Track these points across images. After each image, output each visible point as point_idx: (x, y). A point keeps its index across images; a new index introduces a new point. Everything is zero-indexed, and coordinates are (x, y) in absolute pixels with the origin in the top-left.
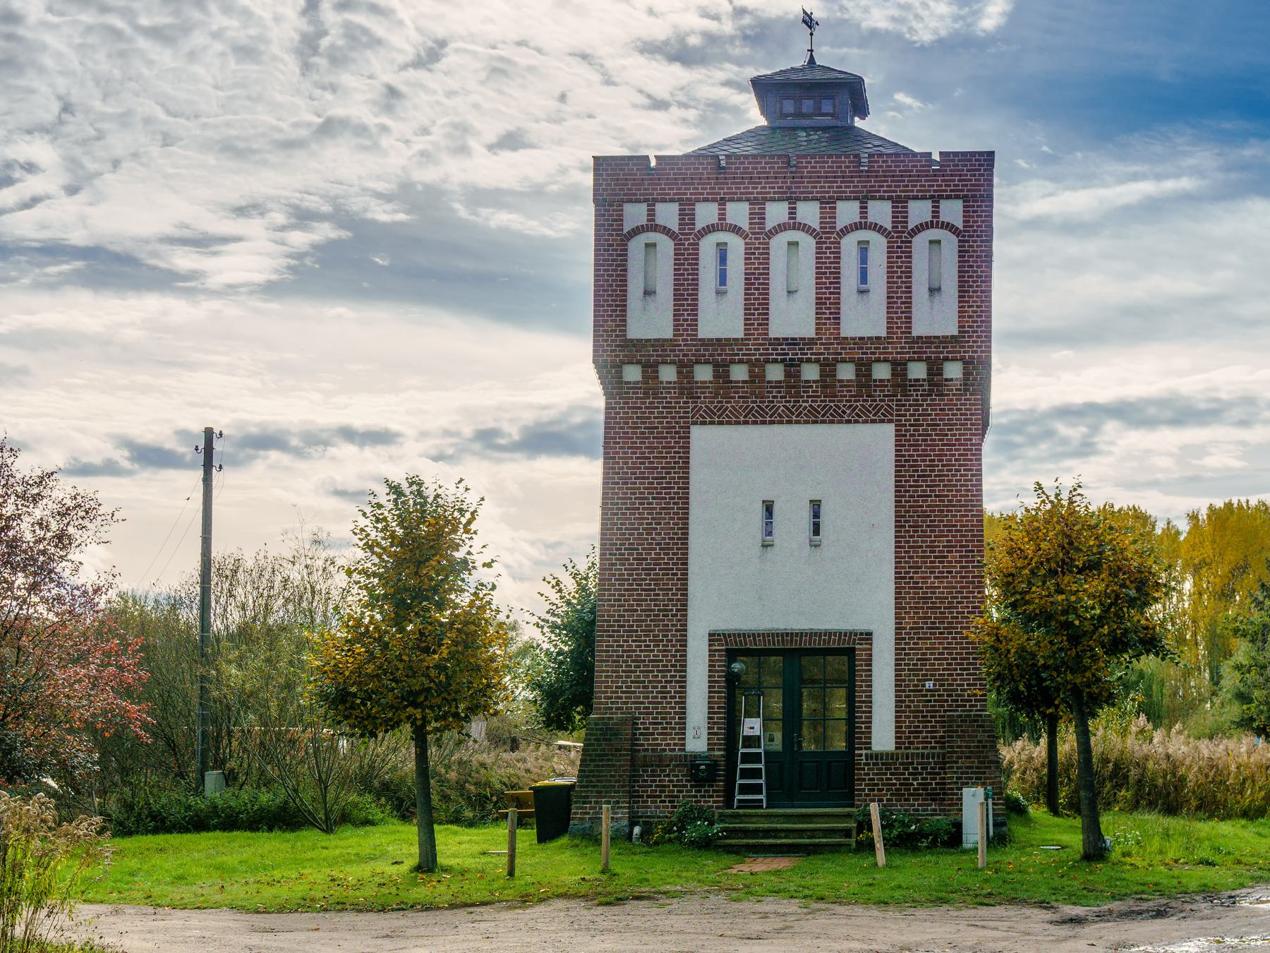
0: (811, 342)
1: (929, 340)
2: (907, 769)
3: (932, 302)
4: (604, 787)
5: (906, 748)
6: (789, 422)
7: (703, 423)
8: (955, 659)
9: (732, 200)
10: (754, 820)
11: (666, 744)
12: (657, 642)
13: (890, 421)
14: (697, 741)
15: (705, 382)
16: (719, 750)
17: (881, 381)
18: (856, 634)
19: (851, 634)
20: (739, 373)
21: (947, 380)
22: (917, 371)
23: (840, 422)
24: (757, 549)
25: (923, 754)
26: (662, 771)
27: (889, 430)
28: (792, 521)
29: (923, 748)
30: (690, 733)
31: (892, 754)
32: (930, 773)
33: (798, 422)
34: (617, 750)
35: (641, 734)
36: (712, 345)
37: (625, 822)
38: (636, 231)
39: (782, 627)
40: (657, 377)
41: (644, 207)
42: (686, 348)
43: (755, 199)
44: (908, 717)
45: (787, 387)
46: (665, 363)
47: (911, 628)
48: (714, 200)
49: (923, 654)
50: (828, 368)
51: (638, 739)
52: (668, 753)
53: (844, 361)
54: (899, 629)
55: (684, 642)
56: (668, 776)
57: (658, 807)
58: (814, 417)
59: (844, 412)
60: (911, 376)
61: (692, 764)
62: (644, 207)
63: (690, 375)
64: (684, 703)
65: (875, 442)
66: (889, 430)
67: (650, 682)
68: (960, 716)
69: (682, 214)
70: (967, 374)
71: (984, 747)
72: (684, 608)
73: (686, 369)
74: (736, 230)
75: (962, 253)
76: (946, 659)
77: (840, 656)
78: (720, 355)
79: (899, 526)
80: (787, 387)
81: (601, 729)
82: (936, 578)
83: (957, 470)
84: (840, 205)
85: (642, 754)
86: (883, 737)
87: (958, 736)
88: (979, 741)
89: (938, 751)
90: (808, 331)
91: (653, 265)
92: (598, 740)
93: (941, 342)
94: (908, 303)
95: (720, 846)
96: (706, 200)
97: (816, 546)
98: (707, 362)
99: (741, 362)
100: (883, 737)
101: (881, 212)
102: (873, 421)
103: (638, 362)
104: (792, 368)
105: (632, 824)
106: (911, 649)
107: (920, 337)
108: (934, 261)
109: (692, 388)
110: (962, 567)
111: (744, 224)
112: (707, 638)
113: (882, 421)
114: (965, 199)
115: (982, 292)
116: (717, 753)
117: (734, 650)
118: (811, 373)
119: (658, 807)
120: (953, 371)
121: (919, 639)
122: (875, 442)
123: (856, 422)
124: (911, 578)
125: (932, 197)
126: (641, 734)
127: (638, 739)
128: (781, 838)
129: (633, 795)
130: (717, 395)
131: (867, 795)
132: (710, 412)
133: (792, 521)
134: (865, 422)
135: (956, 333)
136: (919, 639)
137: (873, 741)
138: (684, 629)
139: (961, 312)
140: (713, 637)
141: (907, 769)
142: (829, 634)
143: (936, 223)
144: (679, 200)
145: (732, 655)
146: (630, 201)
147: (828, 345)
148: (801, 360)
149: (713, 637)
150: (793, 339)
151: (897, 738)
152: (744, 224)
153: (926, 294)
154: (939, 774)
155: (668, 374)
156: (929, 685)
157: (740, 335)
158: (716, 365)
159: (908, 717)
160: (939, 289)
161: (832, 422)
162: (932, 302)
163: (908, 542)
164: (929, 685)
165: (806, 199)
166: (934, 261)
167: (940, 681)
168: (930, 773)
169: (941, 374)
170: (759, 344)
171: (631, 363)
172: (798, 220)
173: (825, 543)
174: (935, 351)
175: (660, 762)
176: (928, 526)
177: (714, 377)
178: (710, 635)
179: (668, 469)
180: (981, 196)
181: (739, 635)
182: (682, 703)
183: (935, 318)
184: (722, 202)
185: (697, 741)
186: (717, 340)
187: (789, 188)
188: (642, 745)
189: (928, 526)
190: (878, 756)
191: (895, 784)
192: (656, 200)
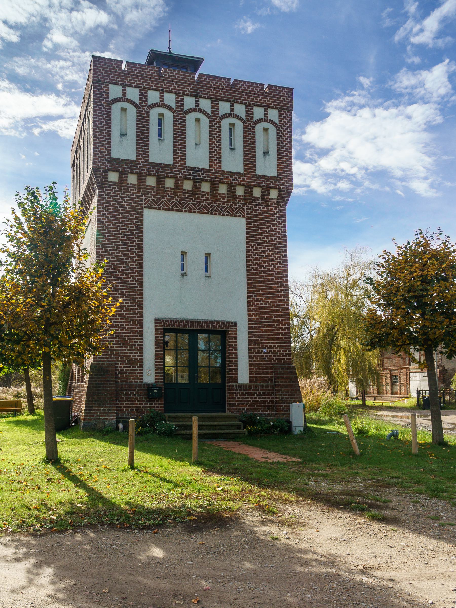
0: (207, 171)
1: (264, 177)
2: (256, 393)
3: (265, 159)
4: (101, 401)
5: (254, 382)
6: (194, 212)
7: (151, 208)
8: (277, 338)
9: (167, 92)
10: (187, 419)
11: (132, 378)
12: (127, 323)
13: (244, 217)
14: (149, 377)
15: (151, 186)
16: (161, 382)
17: (239, 196)
18: (229, 323)
19: (227, 323)
20: (170, 183)
21: (270, 199)
22: (257, 192)
23: (219, 214)
24: (204, 279)
25: (263, 385)
26: (131, 393)
27: (243, 220)
28: (195, 263)
29: (263, 382)
30: (145, 372)
31: (249, 385)
32: (267, 395)
33: (199, 212)
34: (108, 381)
35: (119, 373)
36: (157, 166)
37: (114, 421)
38: (116, 100)
39: (192, 318)
40: (127, 180)
41: (120, 88)
42: (142, 166)
43: (179, 93)
44: (255, 366)
45: (245, 199)
46: (132, 173)
47: (256, 322)
48: (158, 90)
49: (261, 335)
50: (249, 189)
51: (118, 375)
52: (134, 383)
53: (223, 183)
54: (249, 321)
55: (141, 324)
56: (135, 395)
57: (129, 413)
58: (207, 211)
59: (222, 210)
60: (203, 190)
61: (149, 388)
62: (120, 88)
63: (144, 181)
64: (142, 356)
65: (236, 226)
66: (243, 220)
67: (123, 344)
68: (281, 367)
69: (141, 94)
70: (279, 196)
71: (293, 382)
72: (141, 306)
73: (214, 186)
74: (169, 108)
75: (278, 136)
76: (272, 338)
77: (222, 333)
78: (161, 172)
79: (248, 270)
80: (245, 199)
81: (98, 369)
82: (267, 297)
83: (275, 244)
84: (221, 103)
85: (120, 383)
86: (243, 377)
87: (280, 377)
88: (290, 379)
89: (269, 384)
90: (206, 165)
91: (124, 121)
92: (97, 375)
93: (269, 179)
94: (254, 157)
95: (178, 435)
96: (153, 90)
97: (209, 277)
98: (154, 175)
99: (172, 177)
100: (243, 377)
101: (240, 110)
102: (236, 216)
103: (118, 171)
104: (232, 188)
105: (118, 422)
106: (255, 332)
107: (259, 175)
108: (266, 138)
109: (145, 188)
110: (278, 292)
111: (173, 105)
112: (154, 321)
113: (240, 216)
114: (280, 109)
115: (288, 156)
116: (160, 384)
117: (166, 327)
118: (205, 187)
119: (129, 413)
120: (274, 194)
121: (259, 327)
122: (236, 226)
123: (227, 215)
124: (255, 296)
125: (265, 106)
126: (119, 373)
127: (118, 375)
128: (204, 430)
129: (117, 406)
130: (158, 193)
131: (236, 406)
132: (154, 203)
133: (195, 263)
134: (232, 216)
135: (276, 176)
136: (259, 327)
137: (239, 378)
138: (141, 317)
139: (278, 165)
140: (157, 321)
141: (256, 393)
142: (216, 322)
143: (265, 119)
144: (139, 87)
145: (167, 331)
146: (113, 83)
147: (214, 173)
148: (202, 180)
149: (157, 321)
150: (198, 168)
151: (250, 377)
152: (173, 105)
153: (262, 154)
154: (271, 395)
155: (132, 179)
156: (265, 350)
157: (171, 163)
158: (263, 188)
159: (255, 366)
160: (268, 153)
161: (215, 214)
162: (265, 159)
163: (253, 278)
164: (265, 350)
165: (204, 97)
166: (266, 138)
167: (269, 349)
168: (267, 395)
169: (269, 195)
170: (179, 168)
171: (113, 171)
172: (200, 107)
173: (189, 273)
174: (266, 183)
175: (129, 387)
176: (262, 271)
177: (157, 184)
178: (155, 320)
179: (132, 230)
180: (288, 109)
181: (171, 321)
182: (141, 356)
183: (267, 167)
184: (162, 92)
185: (149, 377)
186: (159, 164)
187: (196, 90)
188: (120, 379)
189: (262, 271)
190: (242, 386)
191: (250, 401)
192: (127, 85)
